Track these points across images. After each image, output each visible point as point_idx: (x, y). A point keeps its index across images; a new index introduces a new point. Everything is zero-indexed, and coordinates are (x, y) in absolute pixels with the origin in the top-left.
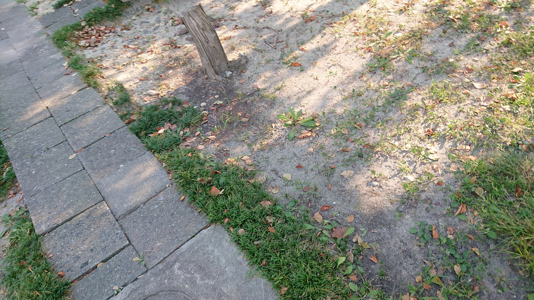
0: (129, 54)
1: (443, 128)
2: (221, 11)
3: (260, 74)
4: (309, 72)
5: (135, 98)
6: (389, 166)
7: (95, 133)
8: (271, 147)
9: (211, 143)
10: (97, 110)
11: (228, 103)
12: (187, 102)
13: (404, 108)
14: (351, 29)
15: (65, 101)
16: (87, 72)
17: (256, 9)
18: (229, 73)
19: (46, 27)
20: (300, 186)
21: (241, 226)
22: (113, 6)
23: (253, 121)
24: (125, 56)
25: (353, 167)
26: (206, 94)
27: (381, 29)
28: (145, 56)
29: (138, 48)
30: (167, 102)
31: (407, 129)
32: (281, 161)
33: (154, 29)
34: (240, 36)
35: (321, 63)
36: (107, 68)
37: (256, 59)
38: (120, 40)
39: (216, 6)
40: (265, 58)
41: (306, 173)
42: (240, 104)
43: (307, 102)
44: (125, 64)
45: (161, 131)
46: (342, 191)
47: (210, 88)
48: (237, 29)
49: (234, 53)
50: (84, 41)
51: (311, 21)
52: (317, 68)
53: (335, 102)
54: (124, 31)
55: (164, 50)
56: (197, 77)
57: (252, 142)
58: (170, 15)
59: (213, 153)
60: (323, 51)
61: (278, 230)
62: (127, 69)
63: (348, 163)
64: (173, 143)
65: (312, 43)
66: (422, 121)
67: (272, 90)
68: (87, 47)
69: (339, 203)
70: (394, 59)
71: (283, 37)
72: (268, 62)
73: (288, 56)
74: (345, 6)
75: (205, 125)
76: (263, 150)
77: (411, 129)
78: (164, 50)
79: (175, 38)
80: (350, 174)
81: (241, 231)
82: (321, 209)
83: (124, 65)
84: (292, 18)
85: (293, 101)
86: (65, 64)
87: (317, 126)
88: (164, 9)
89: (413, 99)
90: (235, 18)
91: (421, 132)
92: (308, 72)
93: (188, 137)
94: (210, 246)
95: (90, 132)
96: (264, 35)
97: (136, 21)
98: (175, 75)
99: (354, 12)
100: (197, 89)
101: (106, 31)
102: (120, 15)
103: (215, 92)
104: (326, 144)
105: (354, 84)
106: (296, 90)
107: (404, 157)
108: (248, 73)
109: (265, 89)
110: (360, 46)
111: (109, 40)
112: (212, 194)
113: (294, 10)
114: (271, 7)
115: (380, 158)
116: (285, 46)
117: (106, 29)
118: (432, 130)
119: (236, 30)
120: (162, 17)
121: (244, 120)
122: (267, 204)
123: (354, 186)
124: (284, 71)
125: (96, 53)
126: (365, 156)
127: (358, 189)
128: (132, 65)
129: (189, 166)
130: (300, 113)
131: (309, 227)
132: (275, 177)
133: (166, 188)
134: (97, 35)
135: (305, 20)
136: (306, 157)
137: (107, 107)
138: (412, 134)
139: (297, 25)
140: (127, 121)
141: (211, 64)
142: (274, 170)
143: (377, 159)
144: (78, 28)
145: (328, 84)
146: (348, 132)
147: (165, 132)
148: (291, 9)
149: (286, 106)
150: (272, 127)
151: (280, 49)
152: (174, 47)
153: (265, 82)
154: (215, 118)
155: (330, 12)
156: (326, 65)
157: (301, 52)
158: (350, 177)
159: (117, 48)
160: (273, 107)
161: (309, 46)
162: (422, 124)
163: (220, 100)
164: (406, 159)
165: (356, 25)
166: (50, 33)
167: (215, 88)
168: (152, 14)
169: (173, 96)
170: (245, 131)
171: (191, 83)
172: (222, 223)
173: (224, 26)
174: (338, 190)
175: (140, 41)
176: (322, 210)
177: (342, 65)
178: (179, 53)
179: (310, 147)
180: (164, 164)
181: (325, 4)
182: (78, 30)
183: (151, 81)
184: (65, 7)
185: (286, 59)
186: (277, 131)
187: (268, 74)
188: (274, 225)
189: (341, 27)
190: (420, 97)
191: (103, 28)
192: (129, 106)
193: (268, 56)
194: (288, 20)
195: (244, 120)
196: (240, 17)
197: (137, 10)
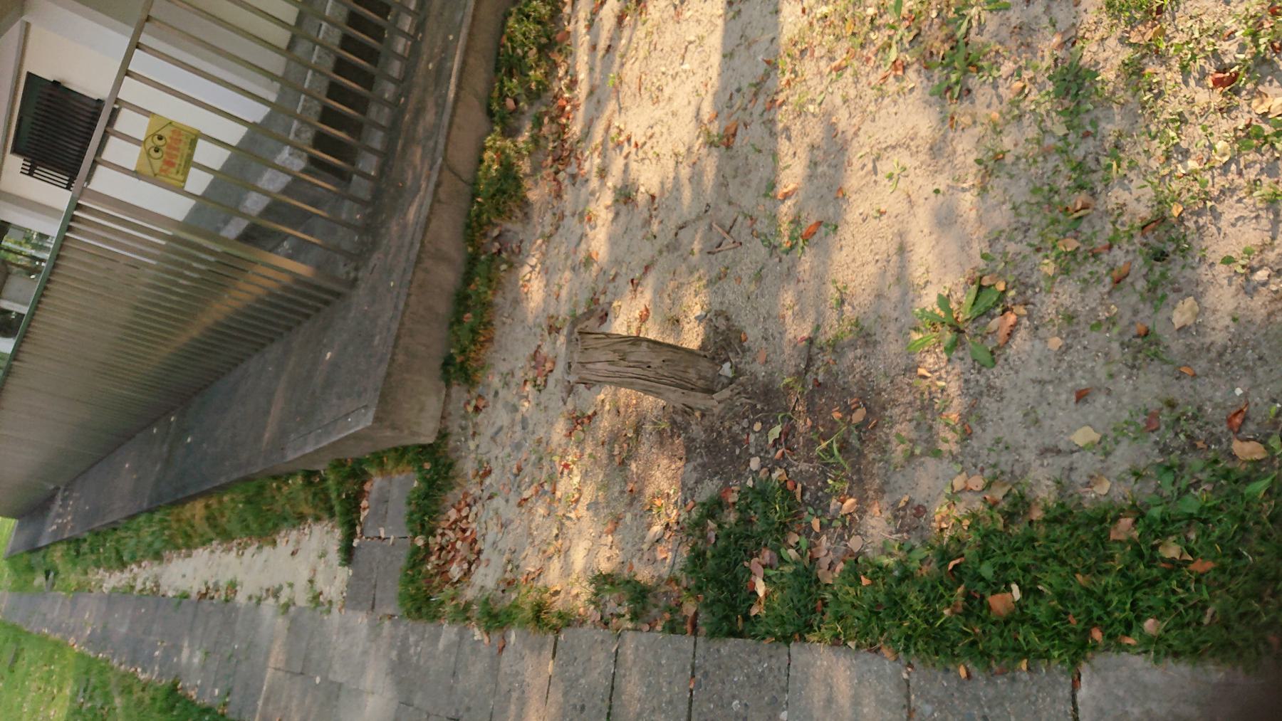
0: (541, 511)
1: (1234, 48)
2: (577, 285)
3: (774, 314)
4: (853, 215)
5: (644, 574)
6: (1238, 219)
7: (670, 702)
8: (973, 416)
9: (861, 518)
10: (620, 658)
11: (791, 419)
12: (727, 488)
13: (1113, 93)
14: (820, 73)
15: (556, 696)
16: (528, 613)
17: (622, 219)
18: (726, 369)
19: (373, 607)
20: (1132, 428)
21: (1139, 619)
22: (427, 466)
23: (874, 407)
24: (538, 520)
25: (1178, 290)
26: (735, 441)
27: (871, 11)
28: (568, 485)
29: (542, 485)
30: (699, 525)
31: (1174, 121)
32: (1032, 420)
33: (524, 428)
34: (658, 292)
35: (853, 180)
36: (541, 572)
37: (731, 296)
38: (498, 502)
39: (561, 287)
40: (745, 279)
41: (1109, 392)
42: (813, 398)
43: (923, 269)
44: (555, 531)
45: (761, 589)
46: (1221, 355)
47: (727, 424)
48: (638, 285)
49: (687, 327)
50: (455, 565)
51: (734, 135)
52: (854, 197)
53: (973, 214)
54: (488, 481)
55: (580, 443)
56: (685, 430)
57: (926, 441)
58: (515, 380)
59: (891, 533)
60: (831, 154)
61: (1213, 554)
62: (570, 536)
63: (1159, 292)
64: (806, 587)
65: (788, 167)
66: (1179, 79)
67: (832, 316)
68: (469, 569)
69: (1246, 381)
70: (968, 30)
71: (727, 213)
72: (759, 277)
73: (779, 234)
74: (755, 47)
75: (807, 496)
76: (967, 435)
77: (1180, 114)
78: (580, 443)
79: (570, 406)
80: (1191, 308)
81: (1150, 625)
82: (1231, 429)
83: (557, 535)
84: (697, 168)
85: (895, 294)
86: (478, 634)
87: (1004, 292)
88: (496, 381)
89: (1106, 60)
90: (613, 273)
91: (1206, 97)
92: (849, 217)
93: (809, 548)
94: (1129, 708)
95: (660, 707)
96: (692, 243)
97: (482, 446)
98: (649, 465)
99: (784, 39)
100: (714, 453)
101: (464, 514)
102: (450, 466)
103: (745, 423)
104: (1068, 303)
105: (959, 149)
106: (872, 269)
107: (1240, 174)
108: (753, 334)
109: (818, 327)
110: (875, 78)
111: (484, 522)
112: (1004, 612)
113: (682, 150)
114: (642, 189)
115: (1201, 221)
116: (749, 222)
117: (459, 511)
118: (1218, 71)
119: (640, 289)
120: (507, 395)
121: (858, 416)
122: (1125, 528)
123: (1228, 321)
124: (806, 262)
125: (492, 564)
126: (1170, 247)
127: (1243, 320)
128: (567, 523)
129: (896, 605)
130: (944, 301)
131: (1259, 487)
132: (1065, 462)
133: (907, 681)
134: (460, 534)
135: (723, 147)
136: (1064, 365)
137: (629, 636)
138: (1192, 119)
139: (719, 169)
140: (688, 627)
141: (686, 388)
142: (1044, 452)
143: (1198, 229)
144: (421, 557)
145: (913, 198)
146: (1076, 238)
147: (766, 579)
148: (676, 155)
149: (895, 315)
150: (925, 377)
151: (749, 238)
152: (586, 421)
153: (800, 315)
154: (804, 466)
155: (745, 85)
156: (863, 173)
157: (789, 203)
158: (1197, 315)
159: (512, 521)
160: (876, 343)
161: (792, 175)
162: (1186, 83)
163: (771, 427)
164: (1251, 174)
165: (817, 54)
166: (390, 611)
167: (737, 417)
168: (489, 409)
169: (690, 503)
170: (887, 435)
171: (689, 450)
172: (1094, 648)
173: (615, 304)
174: (1210, 361)
175: (528, 469)
176: (1237, 431)
177: (891, 141)
178: (605, 423)
179: (1045, 340)
180: (850, 643)
181: (717, 84)
182: (425, 560)
183: (629, 516)
184: (359, 545)
185: (785, 241)
186: (941, 373)
187: (788, 297)
188: (1191, 552)
189: (800, 89)
190: (1112, 42)
191: (453, 514)
192: (655, 596)
193: (746, 269)
194: (696, 178)
195: (858, 416)
196: (617, 262)
197: (464, 428)
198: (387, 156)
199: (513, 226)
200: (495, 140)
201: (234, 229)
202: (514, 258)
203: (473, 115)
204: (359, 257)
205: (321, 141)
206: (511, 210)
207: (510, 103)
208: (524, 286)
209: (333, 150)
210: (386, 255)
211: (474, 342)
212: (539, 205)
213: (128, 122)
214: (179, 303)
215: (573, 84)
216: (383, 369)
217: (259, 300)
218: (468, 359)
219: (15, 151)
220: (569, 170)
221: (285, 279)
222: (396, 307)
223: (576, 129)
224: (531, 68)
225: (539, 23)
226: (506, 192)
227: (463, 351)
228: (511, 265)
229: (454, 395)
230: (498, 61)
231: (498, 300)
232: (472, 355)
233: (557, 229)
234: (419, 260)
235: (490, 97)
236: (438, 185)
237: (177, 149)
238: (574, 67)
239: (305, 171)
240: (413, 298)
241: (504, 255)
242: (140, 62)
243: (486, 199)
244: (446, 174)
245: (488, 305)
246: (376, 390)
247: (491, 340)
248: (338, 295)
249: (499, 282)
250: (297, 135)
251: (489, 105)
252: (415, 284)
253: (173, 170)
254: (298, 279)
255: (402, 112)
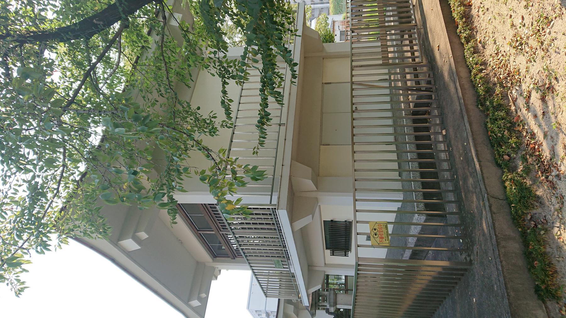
198: (459, 202)
199: (538, 211)
200: (507, 176)
201: (408, 254)
202: (546, 226)
203: (492, 171)
204: (468, 248)
205: (428, 207)
206: (532, 204)
207: (506, 157)
208: (560, 238)
209: (434, 207)
210: (481, 245)
211: (547, 276)
212: (545, 196)
213: (361, 228)
214: (269, 273)
215: (533, 136)
216: (506, 301)
217: (431, 282)
218: (548, 286)
219: (327, 248)
220: (553, 174)
221: (440, 270)
222: (497, 269)
223: (546, 154)
224: (509, 139)
225: (503, 119)
226: (526, 197)
227: (543, 282)
228: (546, 230)
229: (550, 307)
230: (491, 143)
231: (548, 250)
232: (549, 283)
233: (563, 204)
234: (498, 244)
235: (495, 159)
236: (490, 207)
237: (382, 231)
238: (530, 128)
239: (425, 222)
240: (504, 263)
241: (539, 226)
242: (359, 206)
243: (516, 204)
244: (492, 200)
245: (544, 254)
246: (508, 313)
247: (556, 272)
248: (466, 270)
249: (544, 241)
250: (418, 207)
251: (497, 162)
252: (501, 256)
253: (384, 240)
254: (444, 268)
255: (457, 182)
